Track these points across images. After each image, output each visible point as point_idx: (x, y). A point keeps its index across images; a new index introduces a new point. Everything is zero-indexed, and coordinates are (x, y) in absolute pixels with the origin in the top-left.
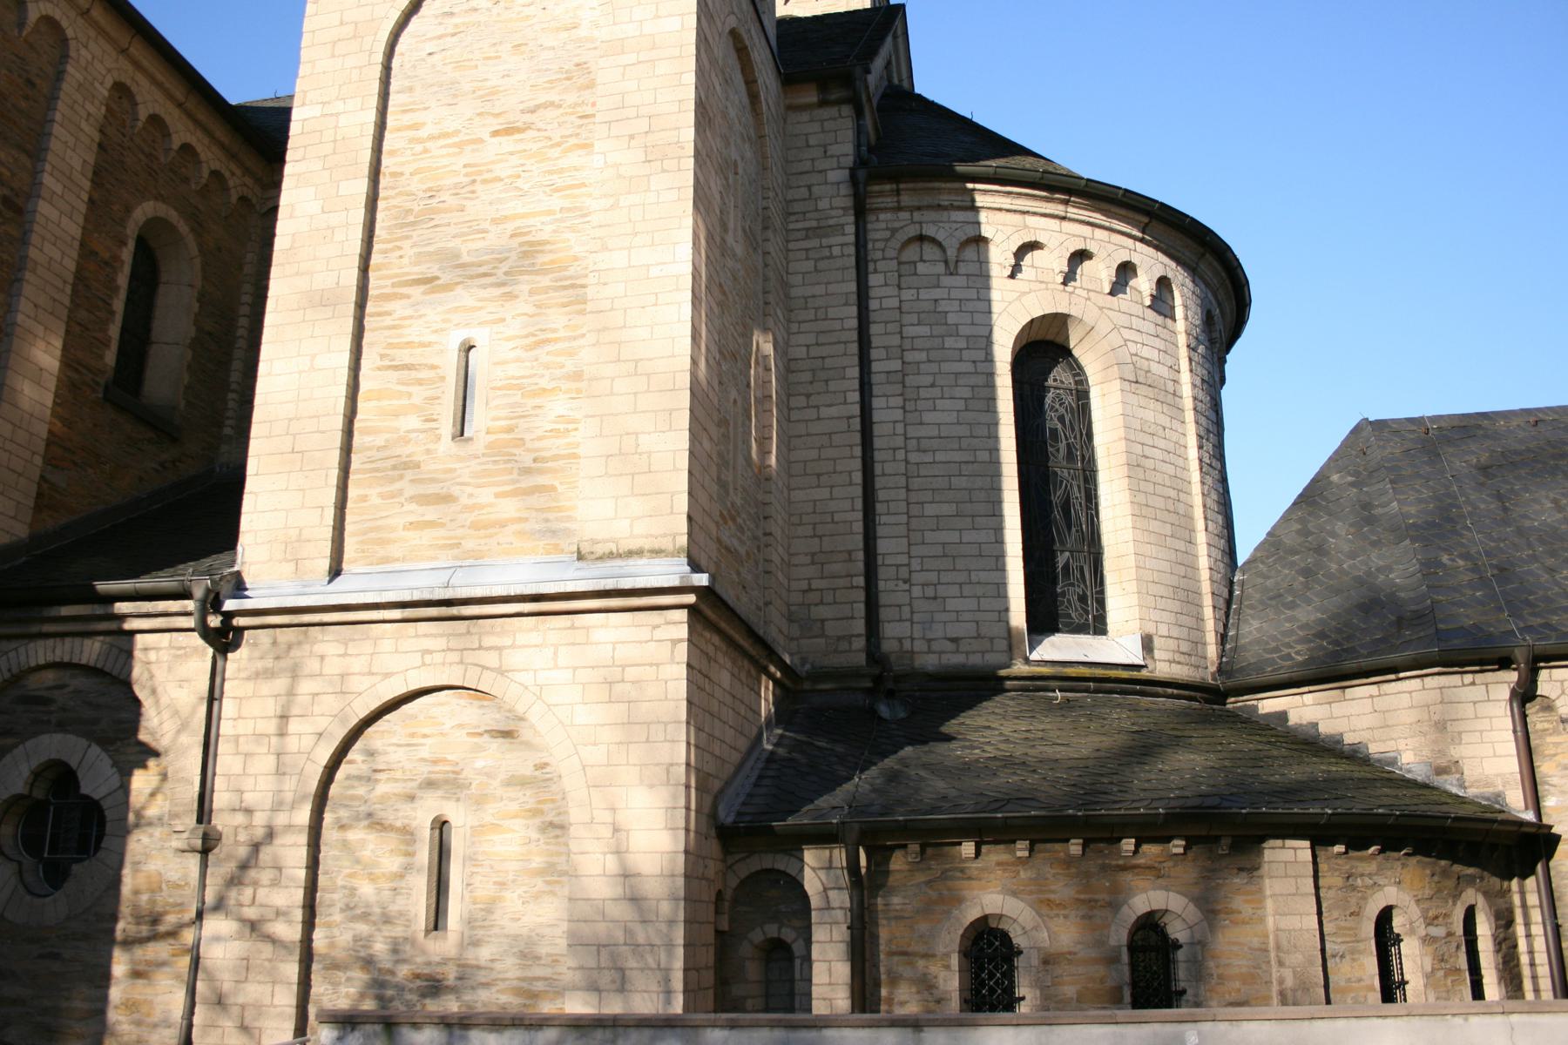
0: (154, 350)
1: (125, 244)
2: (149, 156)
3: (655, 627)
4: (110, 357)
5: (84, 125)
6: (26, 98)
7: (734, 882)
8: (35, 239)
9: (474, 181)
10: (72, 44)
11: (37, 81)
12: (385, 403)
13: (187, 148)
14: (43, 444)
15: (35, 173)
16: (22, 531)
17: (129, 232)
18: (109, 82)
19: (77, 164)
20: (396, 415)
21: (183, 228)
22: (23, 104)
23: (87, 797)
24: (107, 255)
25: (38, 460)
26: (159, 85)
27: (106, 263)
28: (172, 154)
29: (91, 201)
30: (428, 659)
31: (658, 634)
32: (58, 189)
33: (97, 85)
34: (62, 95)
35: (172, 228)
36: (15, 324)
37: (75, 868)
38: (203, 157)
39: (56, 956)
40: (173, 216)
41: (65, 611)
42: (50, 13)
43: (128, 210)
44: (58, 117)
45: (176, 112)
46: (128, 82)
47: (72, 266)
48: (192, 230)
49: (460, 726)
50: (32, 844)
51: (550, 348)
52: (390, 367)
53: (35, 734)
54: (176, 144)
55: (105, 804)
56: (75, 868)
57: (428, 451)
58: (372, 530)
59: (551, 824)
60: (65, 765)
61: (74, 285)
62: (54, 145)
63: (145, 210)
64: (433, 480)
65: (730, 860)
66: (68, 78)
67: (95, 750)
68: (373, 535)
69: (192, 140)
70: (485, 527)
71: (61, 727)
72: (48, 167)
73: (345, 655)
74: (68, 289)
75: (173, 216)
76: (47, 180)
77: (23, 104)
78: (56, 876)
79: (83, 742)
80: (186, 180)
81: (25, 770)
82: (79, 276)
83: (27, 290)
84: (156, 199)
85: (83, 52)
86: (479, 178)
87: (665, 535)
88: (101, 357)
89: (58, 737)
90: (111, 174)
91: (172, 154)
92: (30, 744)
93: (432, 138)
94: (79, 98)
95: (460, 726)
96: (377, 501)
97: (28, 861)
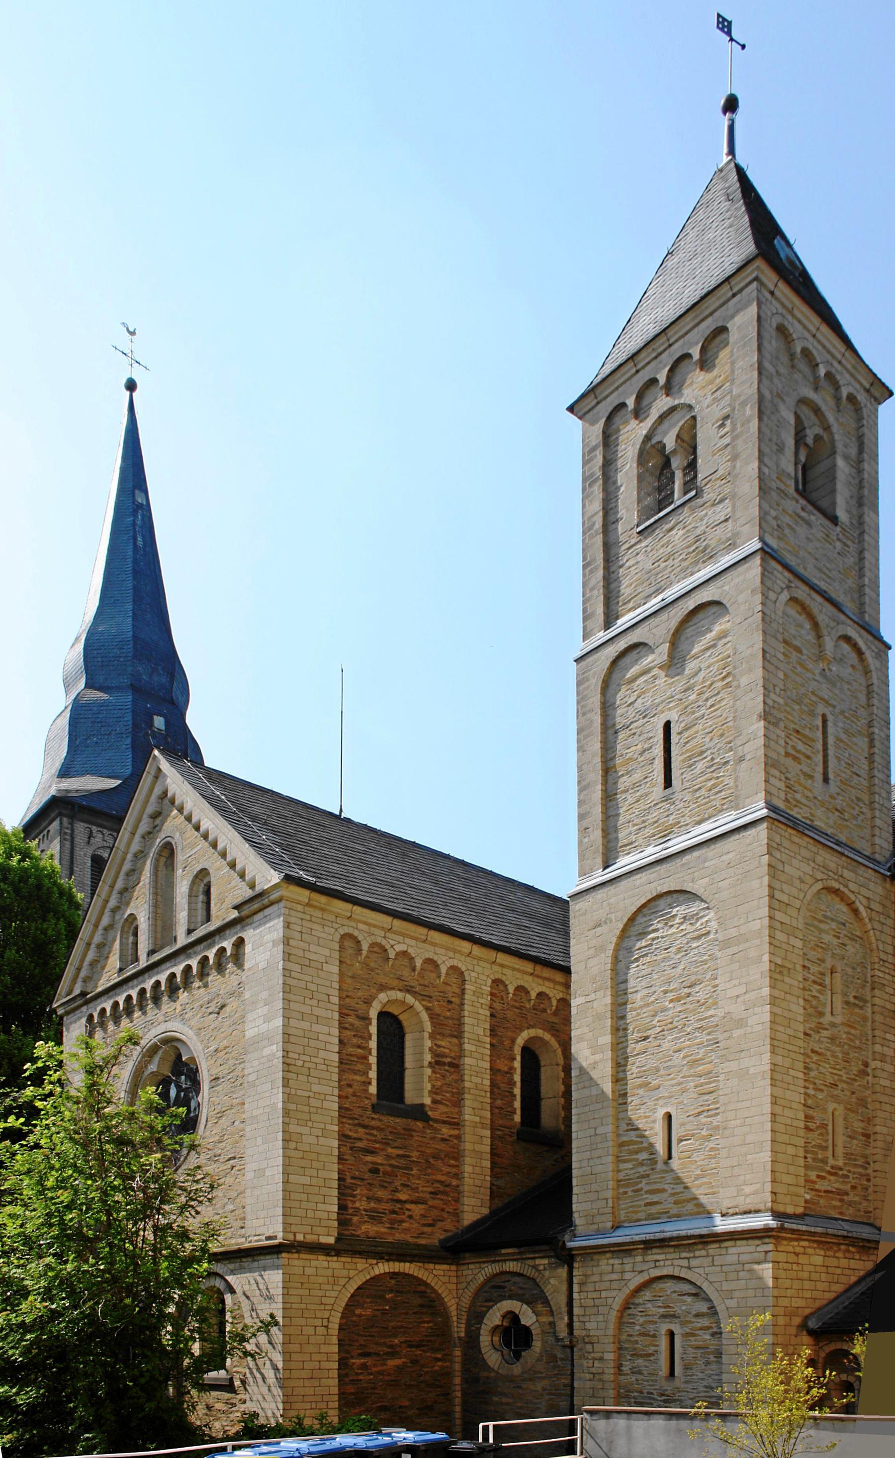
0: (543, 1103)
1: (515, 1059)
2: (520, 1008)
3: (758, 1245)
4: (517, 1118)
5: (481, 1011)
6: (449, 1010)
7: (823, 1355)
8: (466, 1078)
9: (663, 1031)
10: (466, 973)
11: (453, 999)
12: (631, 1147)
13: (540, 995)
14: (489, 1170)
15: (461, 1045)
16: (486, 1211)
17: (516, 1052)
18: (489, 982)
19: (481, 1032)
20: (637, 1153)
21: (547, 1036)
22: (448, 1014)
23: (524, 1326)
24: (506, 1069)
25: (488, 1178)
26: (518, 970)
27: (507, 1073)
28: (532, 1002)
29: (492, 1045)
30: (657, 1264)
31: (759, 1249)
32: (473, 1048)
33: (483, 987)
34: (466, 1001)
35: (541, 1039)
36: (464, 1120)
37: (523, 1353)
38: (551, 995)
39: (520, 1387)
40: (540, 1032)
41: (504, 1251)
42: (452, 964)
43: (513, 1041)
44: (466, 1013)
45: (530, 978)
46: (500, 976)
47: (488, 1083)
48: (553, 1035)
49: (675, 1292)
50: (507, 1344)
51: (705, 1114)
52: (632, 1130)
53: (501, 1301)
54: (533, 995)
55: (532, 1328)
56: (523, 1353)
57: (652, 1169)
58: (631, 1207)
59: (716, 1333)
60: (514, 1313)
61: (492, 1092)
62: (467, 1028)
63: (521, 1040)
64: (655, 1183)
65: (821, 1344)
66: (467, 991)
67: (525, 1306)
68: (631, 1209)
69: (544, 989)
70: (680, 1203)
71: (510, 1298)
72: (466, 1040)
73: (622, 1264)
74: (488, 1095)
75: (540, 1032)
76: (467, 1046)
77: (448, 1014)
78: (517, 1356)
79: (520, 1303)
80: (544, 1010)
81: (498, 1315)
82: (493, 1084)
83: (468, 1103)
84: (528, 1028)
85: (473, 974)
86: (666, 1028)
87: (760, 1203)
88: (513, 1119)
89: (509, 1302)
90: (499, 1028)
91: (532, 1002)
92: (499, 1305)
93: (641, 1007)
94: (475, 999)
95: (675, 1292)
96: (630, 1194)
97: (506, 1351)
